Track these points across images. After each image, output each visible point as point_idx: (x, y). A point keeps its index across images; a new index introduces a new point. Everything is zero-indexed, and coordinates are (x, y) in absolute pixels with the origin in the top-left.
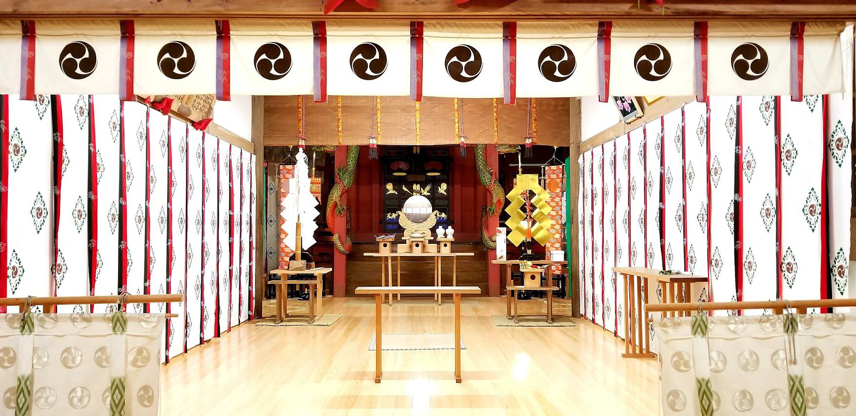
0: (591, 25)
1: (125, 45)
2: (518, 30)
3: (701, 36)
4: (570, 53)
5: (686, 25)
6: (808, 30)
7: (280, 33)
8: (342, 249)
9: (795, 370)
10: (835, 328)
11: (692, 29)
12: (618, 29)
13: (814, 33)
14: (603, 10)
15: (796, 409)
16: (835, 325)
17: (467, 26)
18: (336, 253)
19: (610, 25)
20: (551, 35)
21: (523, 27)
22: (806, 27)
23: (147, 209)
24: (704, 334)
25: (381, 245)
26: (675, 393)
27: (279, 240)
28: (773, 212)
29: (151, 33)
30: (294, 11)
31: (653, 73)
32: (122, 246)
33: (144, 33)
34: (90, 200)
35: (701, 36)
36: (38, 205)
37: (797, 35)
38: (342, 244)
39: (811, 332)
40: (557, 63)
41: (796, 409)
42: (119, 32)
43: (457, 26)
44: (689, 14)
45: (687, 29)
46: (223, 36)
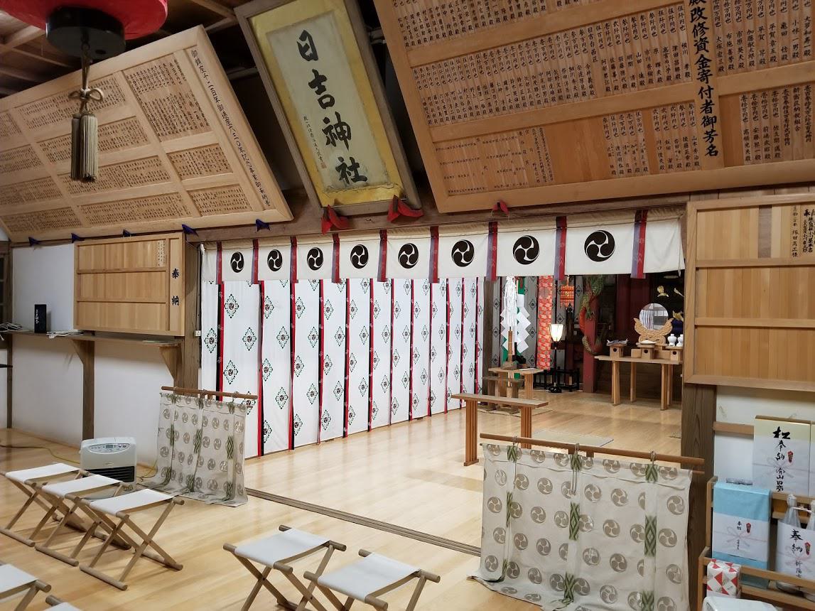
0: (484, 225)
1: (433, 243)
2: (439, 231)
3: (562, 228)
4: (471, 246)
5: (550, 220)
6: (650, 217)
7: (319, 242)
8: (589, 349)
9: (576, 499)
10: (610, 472)
11: (555, 223)
12: (502, 226)
13: (657, 218)
14: (621, 205)
15: (653, 529)
16: (612, 470)
17: (449, 228)
18: (585, 352)
19: (496, 224)
20: (459, 234)
21: (442, 229)
22: (649, 214)
23: (462, 326)
24: (515, 461)
25: (611, 350)
26: (494, 499)
27: (500, 345)
28: (408, 380)
29: (447, 235)
30: (309, 232)
31: (526, 258)
32: (219, 361)
33: (574, 225)
34: (320, 329)
35: (562, 228)
36: (249, 334)
37: (641, 223)
38: (590, 345)
39: (591, 472)
40: (526, 250)
41: (653, 529)
42: (252, 246)
43: (464, 227)
44: (553, 214)
45: (551, 223)
46: (256, 249)
